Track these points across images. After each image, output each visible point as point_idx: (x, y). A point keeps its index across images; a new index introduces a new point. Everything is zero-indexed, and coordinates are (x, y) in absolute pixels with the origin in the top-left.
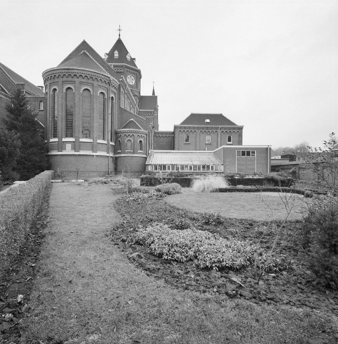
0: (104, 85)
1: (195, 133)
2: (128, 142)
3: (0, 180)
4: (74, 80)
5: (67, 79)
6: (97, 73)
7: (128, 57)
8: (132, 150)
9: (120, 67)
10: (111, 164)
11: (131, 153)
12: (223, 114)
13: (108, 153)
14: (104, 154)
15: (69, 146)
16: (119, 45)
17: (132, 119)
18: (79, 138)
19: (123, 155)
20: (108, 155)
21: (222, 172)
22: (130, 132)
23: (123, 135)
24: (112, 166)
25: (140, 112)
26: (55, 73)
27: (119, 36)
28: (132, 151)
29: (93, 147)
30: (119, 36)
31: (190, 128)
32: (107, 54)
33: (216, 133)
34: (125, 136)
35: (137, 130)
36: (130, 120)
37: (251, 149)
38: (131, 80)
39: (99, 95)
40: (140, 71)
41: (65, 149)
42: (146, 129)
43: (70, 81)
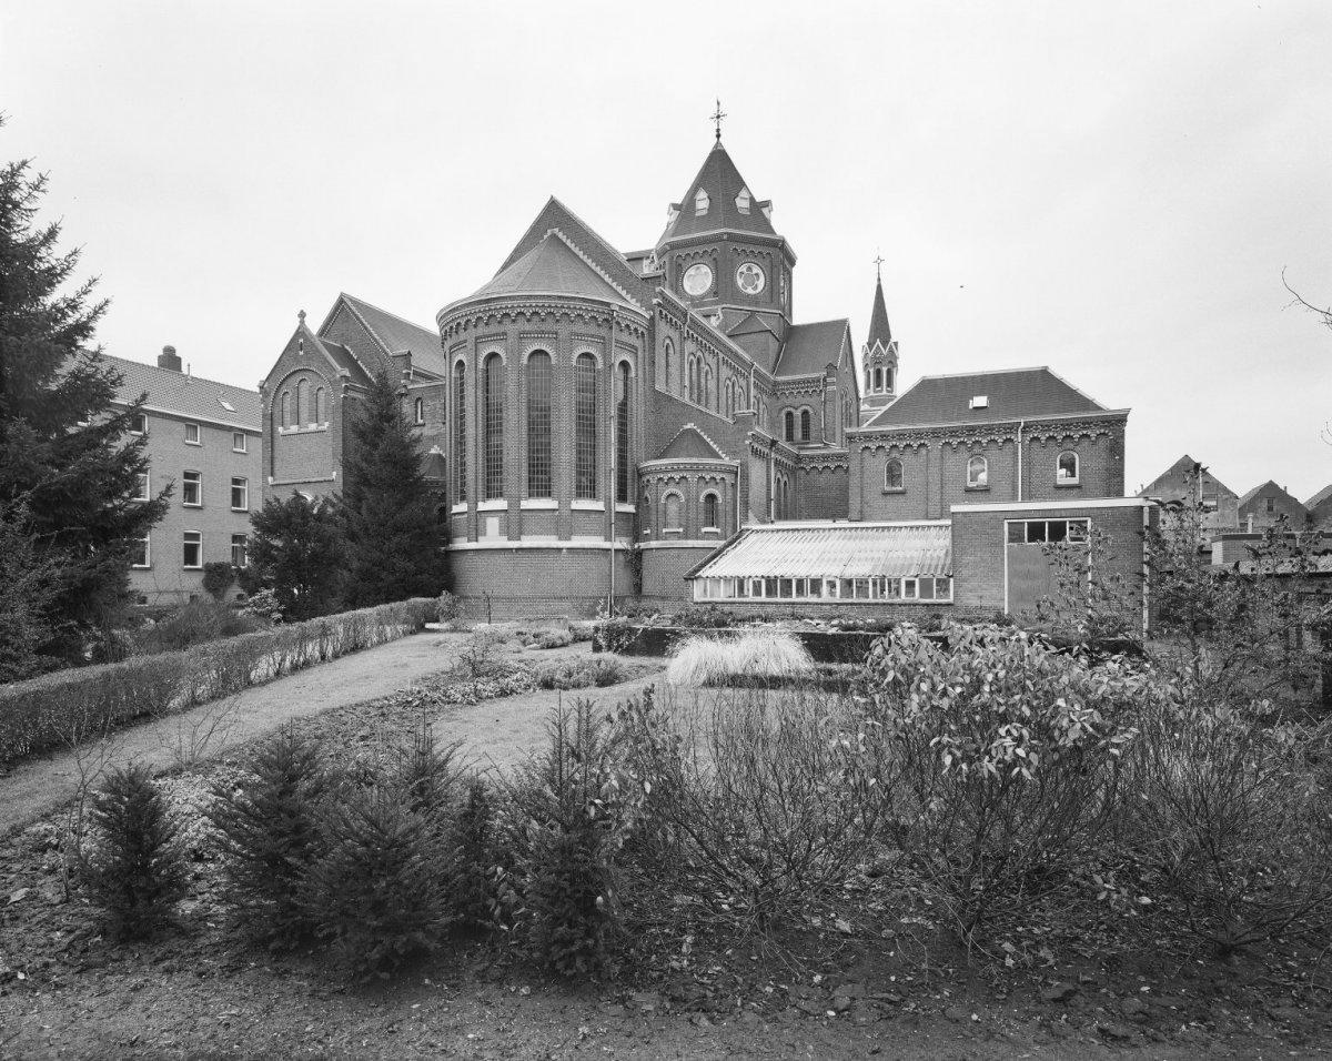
0: (593, 329)
1: (924, 451)
2: (670, 501)
4: (501, 329)
5: (487, 331)
6: (567, 298)
7: (742, 203)
8: (680, 526)
9: (711, 242)
10: (621, 571)
12: (1058, 371)
13: (608, 539)
14: (598, 542)
15: (493, 524)
16: (720, 172)
17: (690, 426)
18: (520, 499)
19: (654, 544)
20: (607, 545)
21: (949, 605)
22: (673, 470)
23: (653, 479)
24: (621, 580)
25: (776, 384)
26: (507, 307)
27: (718, 136)
28: (681, 530)
29: (563, 524)
30: (718, 136)
31: (901, 435)
32: (676, 207)
33: (1010, 445)
35: (711, 461)
36: (686, 427)
37: (1016, 515)
38: (751, 279)
39: (578, 362)
40: (784, 241)
42: (733, 454)
43: (494, 335)
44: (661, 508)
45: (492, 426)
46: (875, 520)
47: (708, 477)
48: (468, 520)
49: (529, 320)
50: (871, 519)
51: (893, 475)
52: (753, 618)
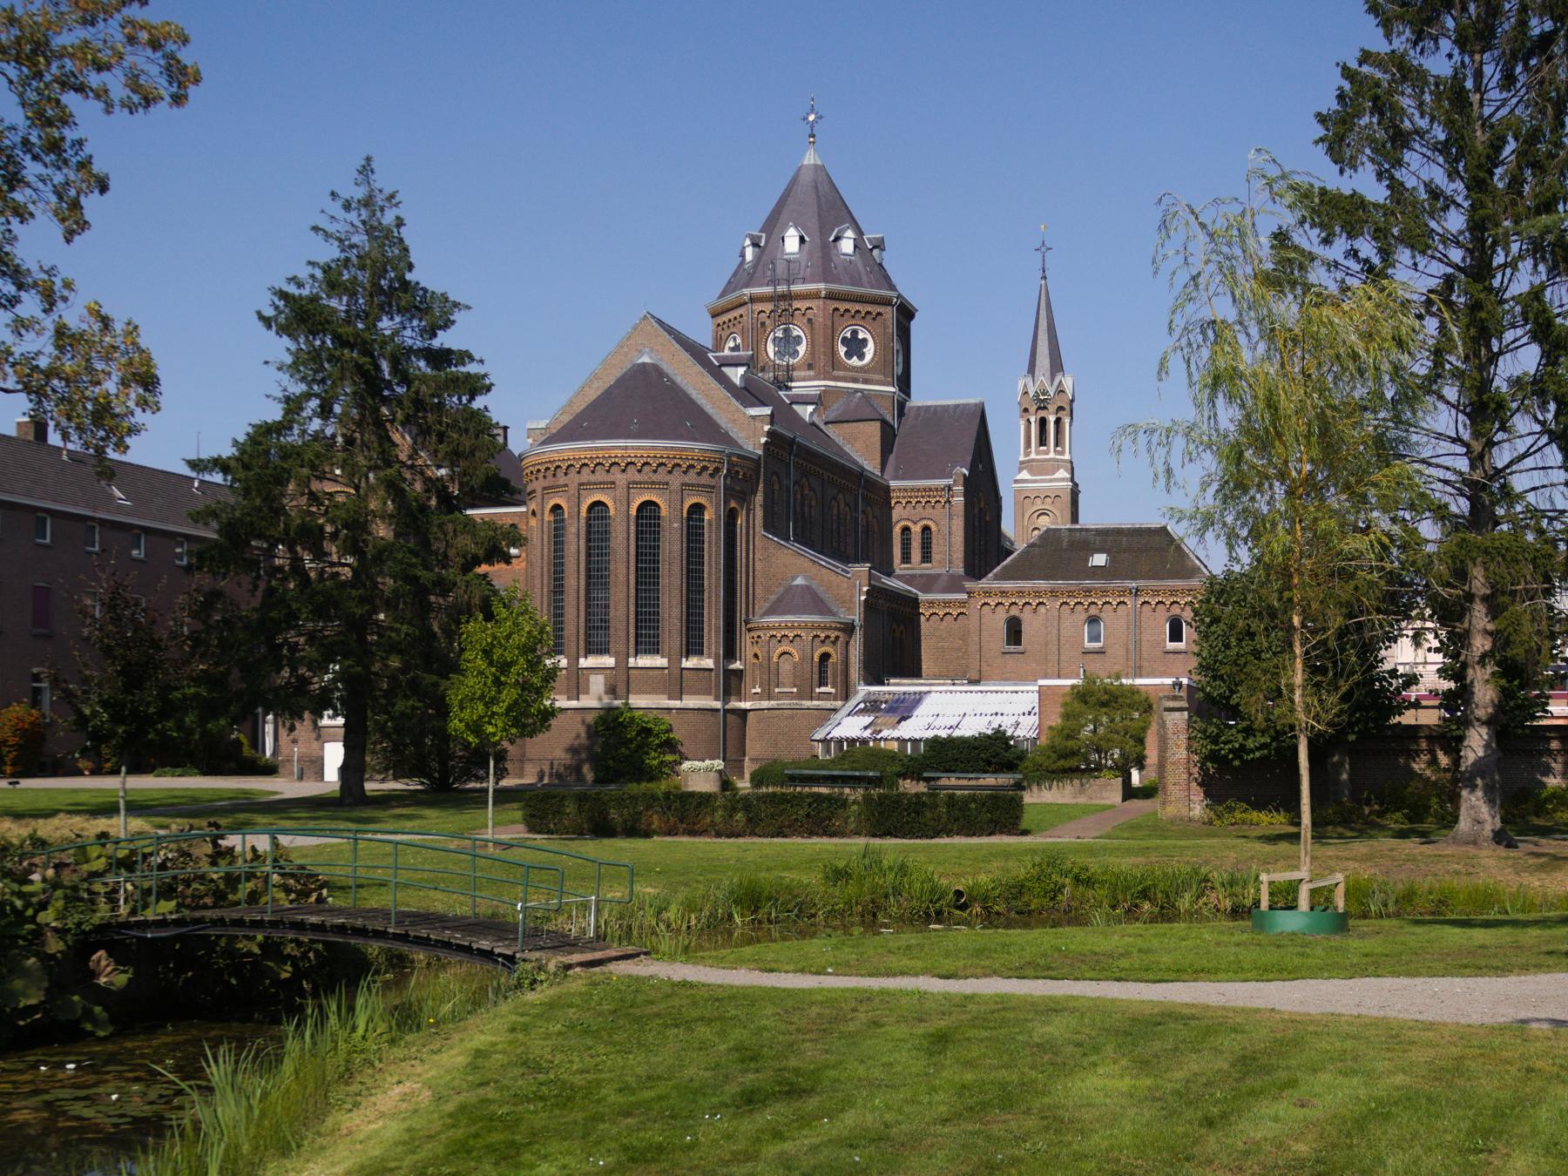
1: (1042, 609)
3: (7, 6)
4: (610, 478)
5: (593, 478)
11: (790, 695)
22: (787, 627)
29: (677, 683)
31: (1021, 593)
34: (774, 641)
45: (596, 575)
47: (823, 635)
51: (1014, 631)
52: (638, 955)
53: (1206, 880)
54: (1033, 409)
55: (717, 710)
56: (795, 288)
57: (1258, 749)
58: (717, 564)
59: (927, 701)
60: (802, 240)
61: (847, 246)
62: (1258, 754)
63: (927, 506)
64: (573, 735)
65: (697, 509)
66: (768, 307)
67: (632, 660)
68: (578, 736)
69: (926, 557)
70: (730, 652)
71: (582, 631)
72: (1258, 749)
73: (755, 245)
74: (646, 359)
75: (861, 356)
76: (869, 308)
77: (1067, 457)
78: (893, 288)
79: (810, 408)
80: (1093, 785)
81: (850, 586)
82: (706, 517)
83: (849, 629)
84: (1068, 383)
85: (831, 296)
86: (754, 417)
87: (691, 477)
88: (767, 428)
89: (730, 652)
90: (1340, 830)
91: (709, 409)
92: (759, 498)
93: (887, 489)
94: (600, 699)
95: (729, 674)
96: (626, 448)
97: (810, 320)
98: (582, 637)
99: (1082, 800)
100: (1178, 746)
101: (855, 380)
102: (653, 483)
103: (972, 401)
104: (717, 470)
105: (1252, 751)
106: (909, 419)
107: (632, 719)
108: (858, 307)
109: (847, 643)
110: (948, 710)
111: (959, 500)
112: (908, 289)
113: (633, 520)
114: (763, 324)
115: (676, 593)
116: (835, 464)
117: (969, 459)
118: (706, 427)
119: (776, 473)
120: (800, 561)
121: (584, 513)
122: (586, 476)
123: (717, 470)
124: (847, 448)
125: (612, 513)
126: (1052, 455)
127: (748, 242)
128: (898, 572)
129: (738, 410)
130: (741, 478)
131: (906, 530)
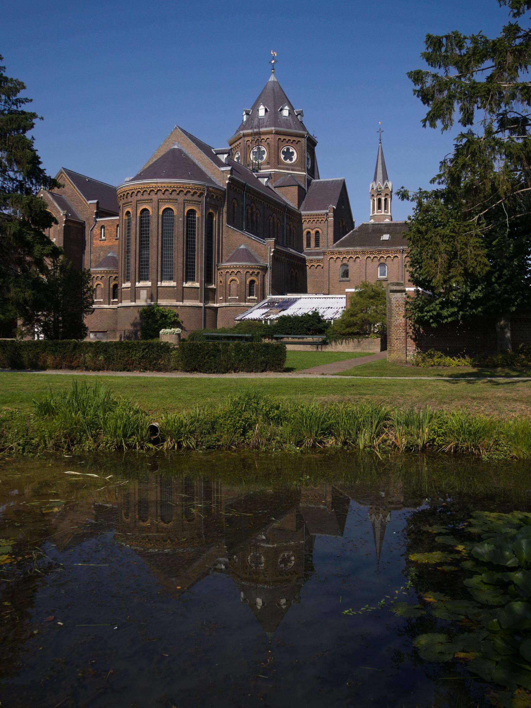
1: (358, 260)
2: (232, 283)
5: (142, 198)
8: (237, 296)
31: (348, 253)
34: (228, 274)
41: (139, 299)
44: (228, 286)
45: (144, 243)
46: (336, 294)
47: (251, 272)
48: (131, 291)
49: (164, 194)
50: (332, 294)
53: (386, 418)
54: (375, 195)
55: (202, 307)
56: (262, 130)
57: (450, 316)
58: (202, 238)
59: (299, 302)
60: (266, 111)
61: (285, 113)
62: (450, 320)
63: (317, 221)
64: (133, 319)
65: (192, 212)
66: (250, 138)
67: (159, 283)
68: (136, 318)
69: (317, 245)
70: (209, 278)
71: (137, 270)
72: (450, 316)
73: (247, 114)
74: (176, 147)
75: (291, 159)
76: (295, 139)
77: (389, 214)
78: (305, 129)
79: (266, 179)
80: (365, 342)
81: (266, 249)
82: (197, 216)
83: (264, 269)
84: (390, 185)
85: (277, 133)
86: (223, 171)
87: (189, 197)
88: (229, 176)
89: (209, 278)
90: (507, 370)
91: (204, 169)
92: (225, 209)
93: (300, 215)
94: (146, 301)
95: (207, 290)
96: (157, 183)
97: (268, 143)
98: (137, 272)
99: (359, 350)
100: (399, 315)
101: (288, 169)
102: (170, 199)
103: (340, 179)
104: (202, 194)
105: (446, 317)
106: (312, 187)
107: (158, 310)
108: (289, 138)
109: (264, 276)
110: (303, 305)
111: (331, 219)
112: (312, 130)
113: (160, 217)
114: (249, 146)
115: (181, 251)
116: (271, 200)
117: (337, 202)
118: (196, 172)
119: (235, 198)
120: (243, 238)
121: (138, 215)
122: (139, 197)
123: (202, 194)
124: (284, 198)
125: (151, 214)
126: (383, 213)
127: (244, 113)
128: (305, 251)
129: (216, 168)
130: (214, 198)
131: (308, 233)
